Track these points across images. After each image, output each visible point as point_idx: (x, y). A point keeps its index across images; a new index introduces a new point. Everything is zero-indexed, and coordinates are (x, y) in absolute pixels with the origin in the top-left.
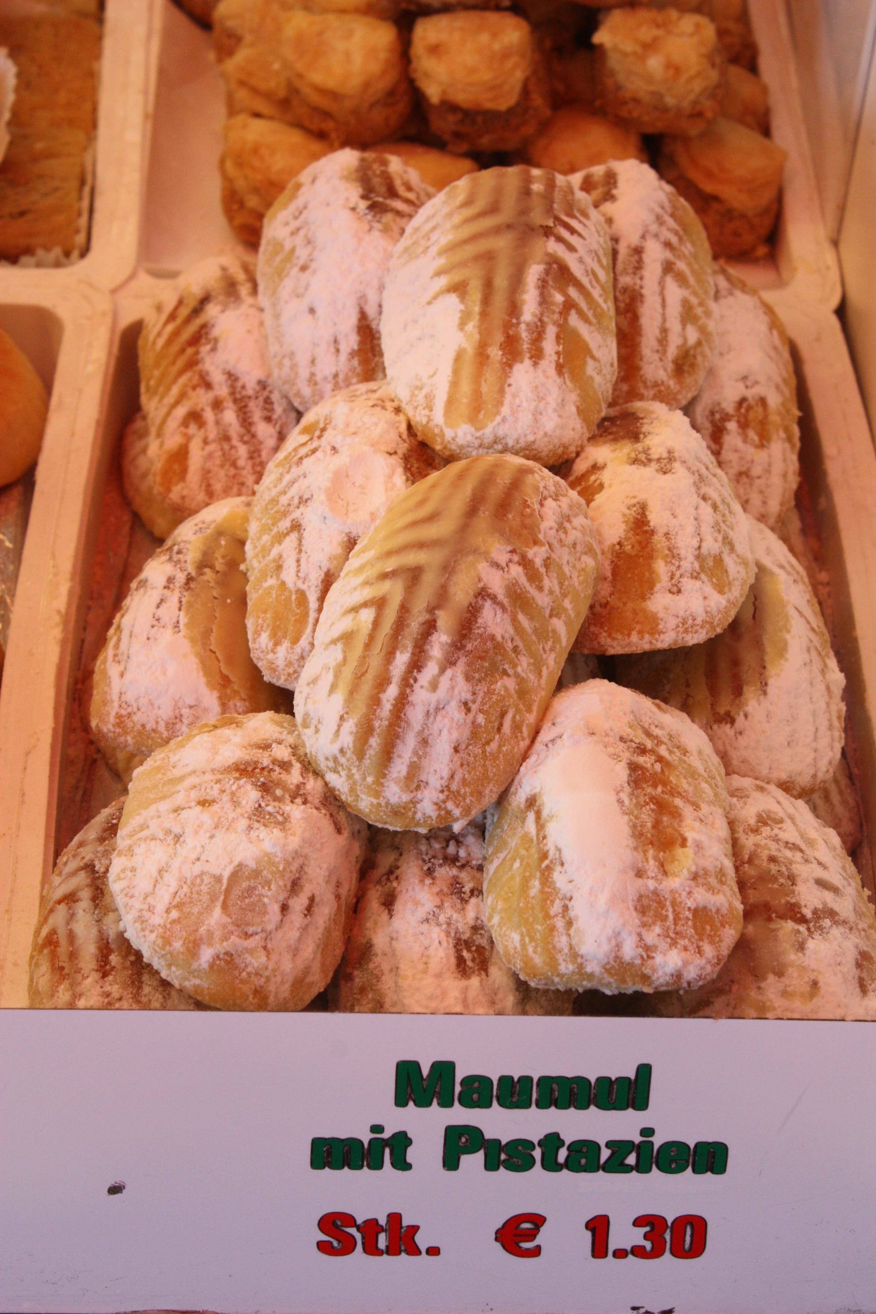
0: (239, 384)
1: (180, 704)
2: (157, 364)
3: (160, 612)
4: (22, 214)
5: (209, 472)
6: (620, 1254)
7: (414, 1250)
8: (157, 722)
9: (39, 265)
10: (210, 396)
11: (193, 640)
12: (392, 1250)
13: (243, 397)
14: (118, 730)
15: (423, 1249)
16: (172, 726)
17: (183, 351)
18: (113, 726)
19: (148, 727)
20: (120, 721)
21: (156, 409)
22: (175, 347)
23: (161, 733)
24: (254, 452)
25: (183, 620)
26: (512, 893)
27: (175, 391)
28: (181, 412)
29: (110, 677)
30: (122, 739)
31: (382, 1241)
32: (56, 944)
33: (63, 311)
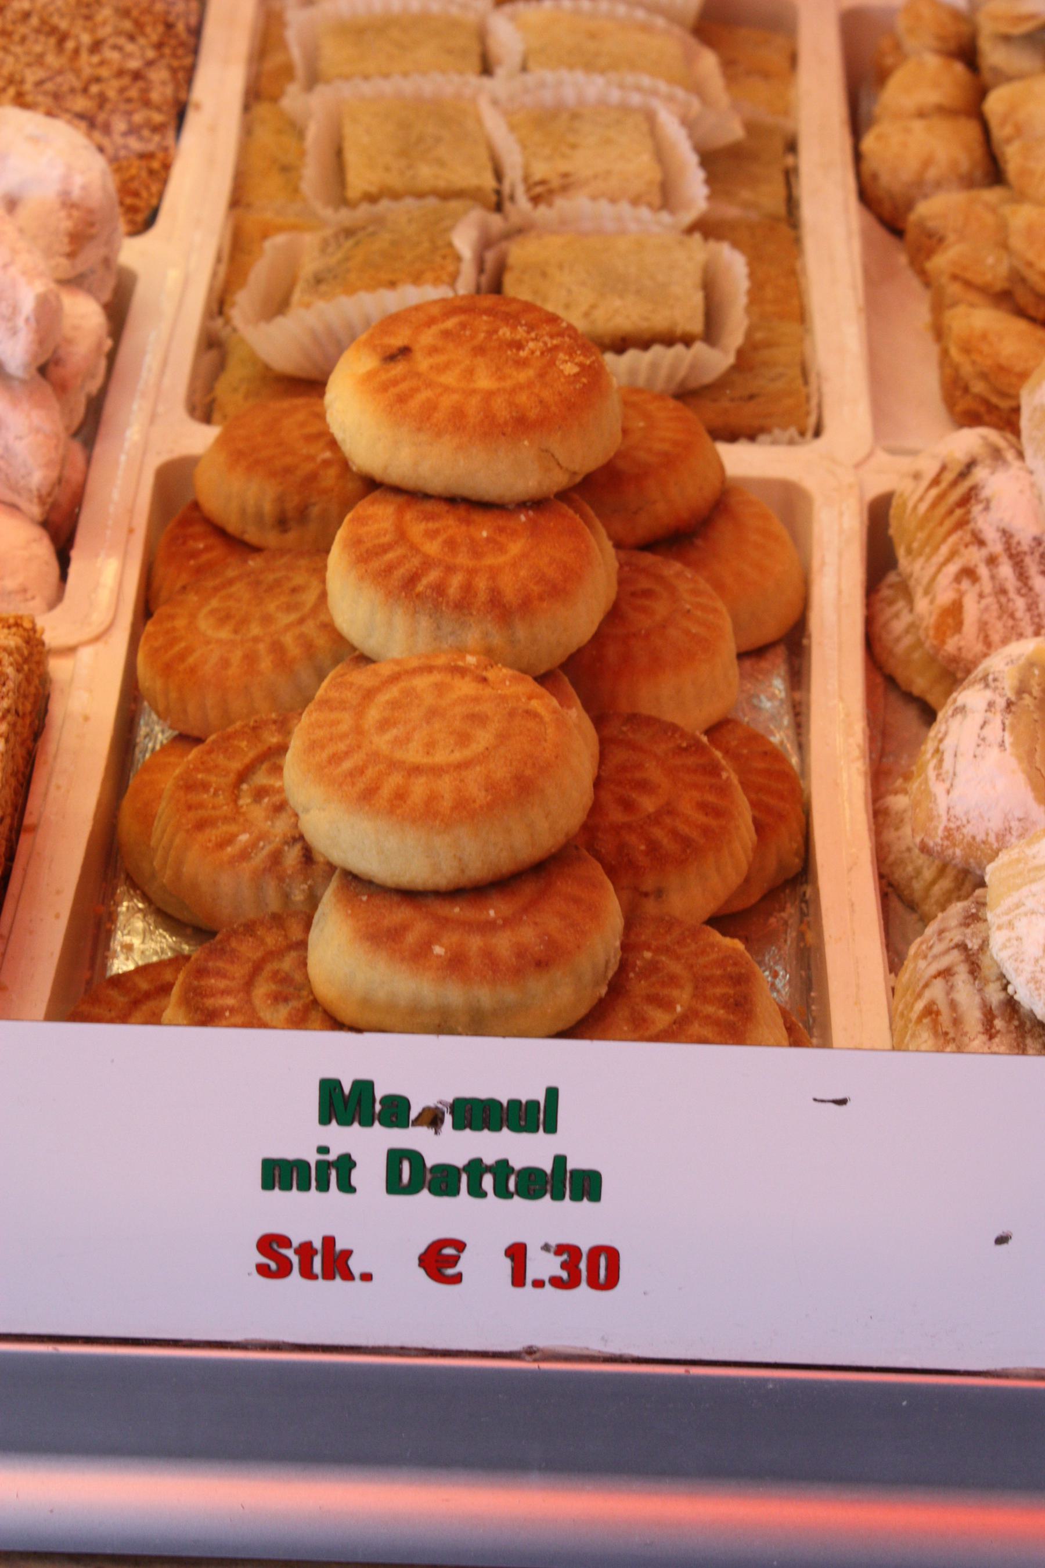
0: (1014, 541)
1: (1010, 816)
2: (921, 526)
3: (986, 732)
4: (751, 397)
5: (986, 623)
6: (538, 1284)
7: (348, 1276)
8: (987, 834)
9: (774, 442)
10: (984, 552)
11: (1019, 759)
12: (328, 1275)
13: (1018, 554)
14: (946, 843)
16: (1001, 837)
17: (951, 512)
18: (942, 839)
19: (978, 839)
20: (949, 834)
21: (923, 568)
22: (942, 509)
23: (991, 845)
24: (1032, 604)
25: (1008, 739)
27: (944, 550)
28: (952, 569)
29: (935, 795)
30: (950, 852)
32: (938, 1013)
33: (810, 483)
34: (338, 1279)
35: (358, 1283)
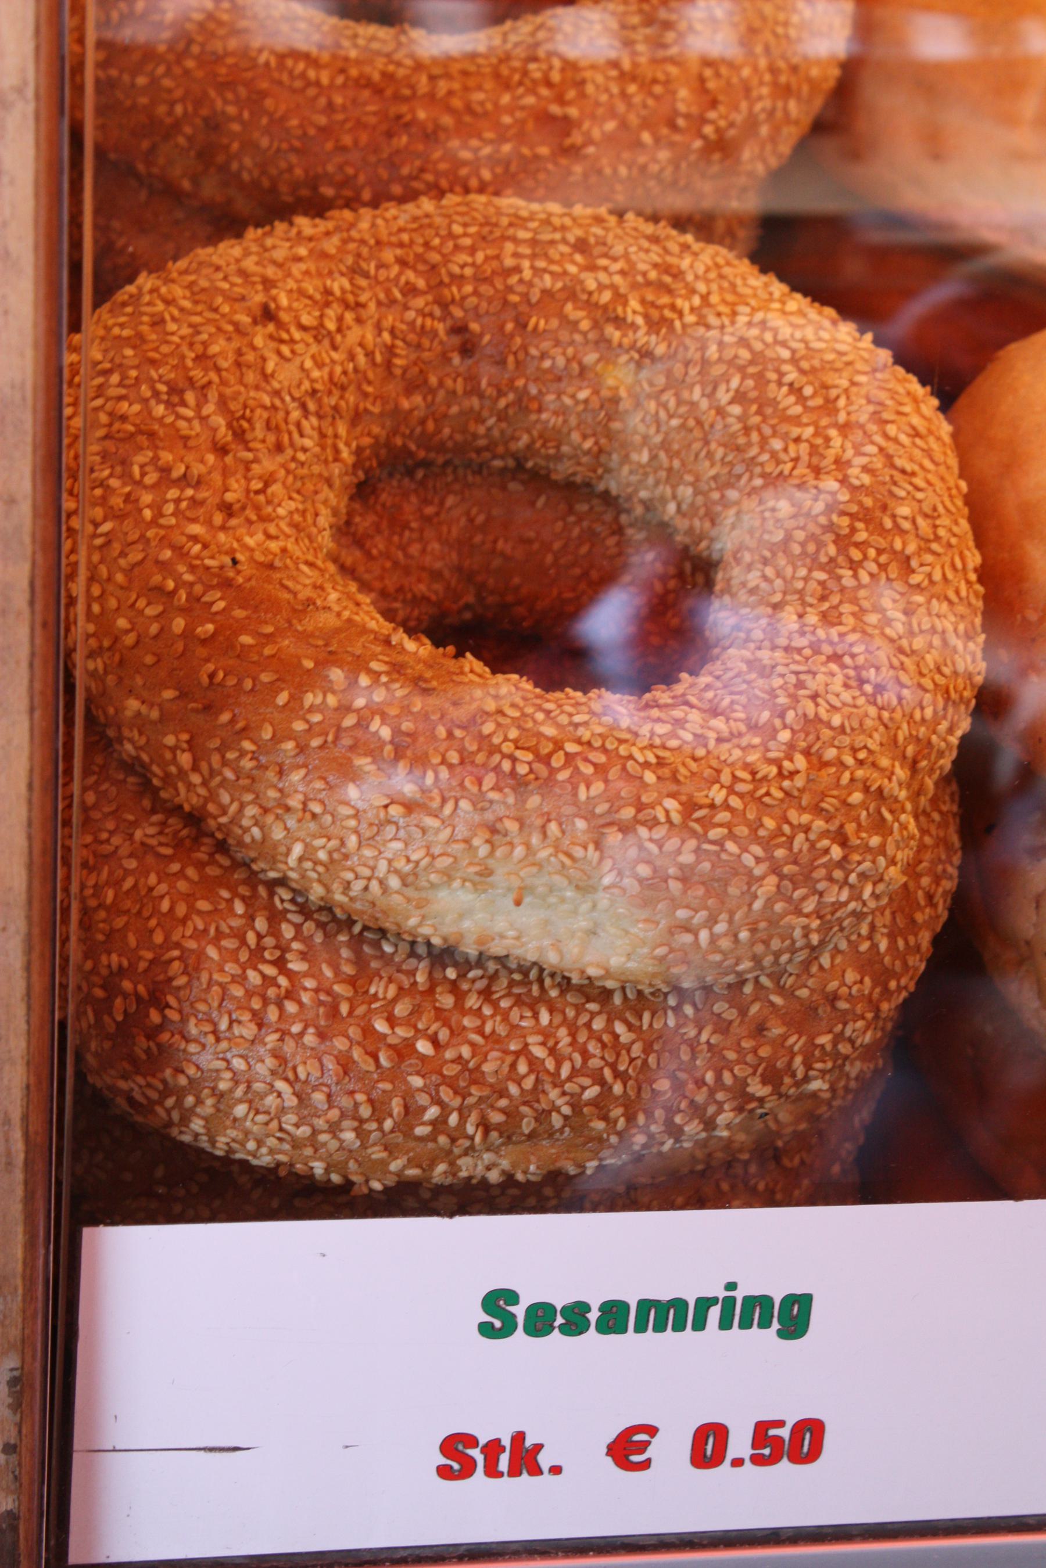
6: (738, 1463)
7: (535, 1470)
12: (514, 1471)
15: (545, 1468)
26: (428, 519)
31: (504, 1462)
34: (525, 1475)
35: (546, 1476)
